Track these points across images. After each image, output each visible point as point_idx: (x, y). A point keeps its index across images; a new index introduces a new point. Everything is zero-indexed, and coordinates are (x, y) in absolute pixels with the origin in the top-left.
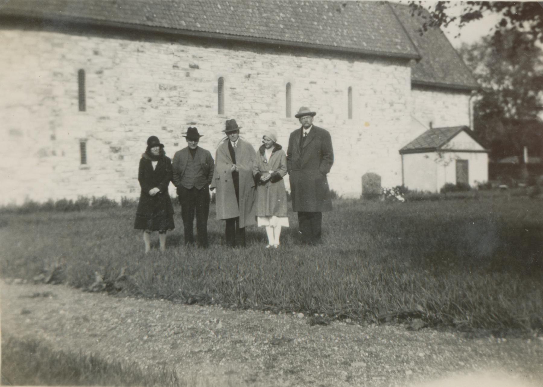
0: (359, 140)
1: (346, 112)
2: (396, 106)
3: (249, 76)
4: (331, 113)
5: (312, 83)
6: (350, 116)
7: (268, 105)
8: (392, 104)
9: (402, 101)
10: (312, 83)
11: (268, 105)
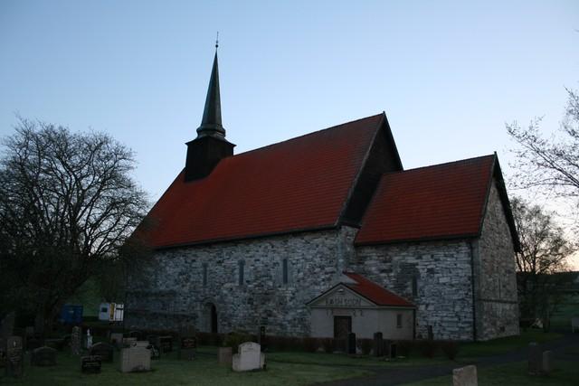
1: (281, 276)
3: (219, 262)
5: (256, 260)
6: (285, 280)
8: (322, 268)
10: (256, 260)
11: (229, 278)
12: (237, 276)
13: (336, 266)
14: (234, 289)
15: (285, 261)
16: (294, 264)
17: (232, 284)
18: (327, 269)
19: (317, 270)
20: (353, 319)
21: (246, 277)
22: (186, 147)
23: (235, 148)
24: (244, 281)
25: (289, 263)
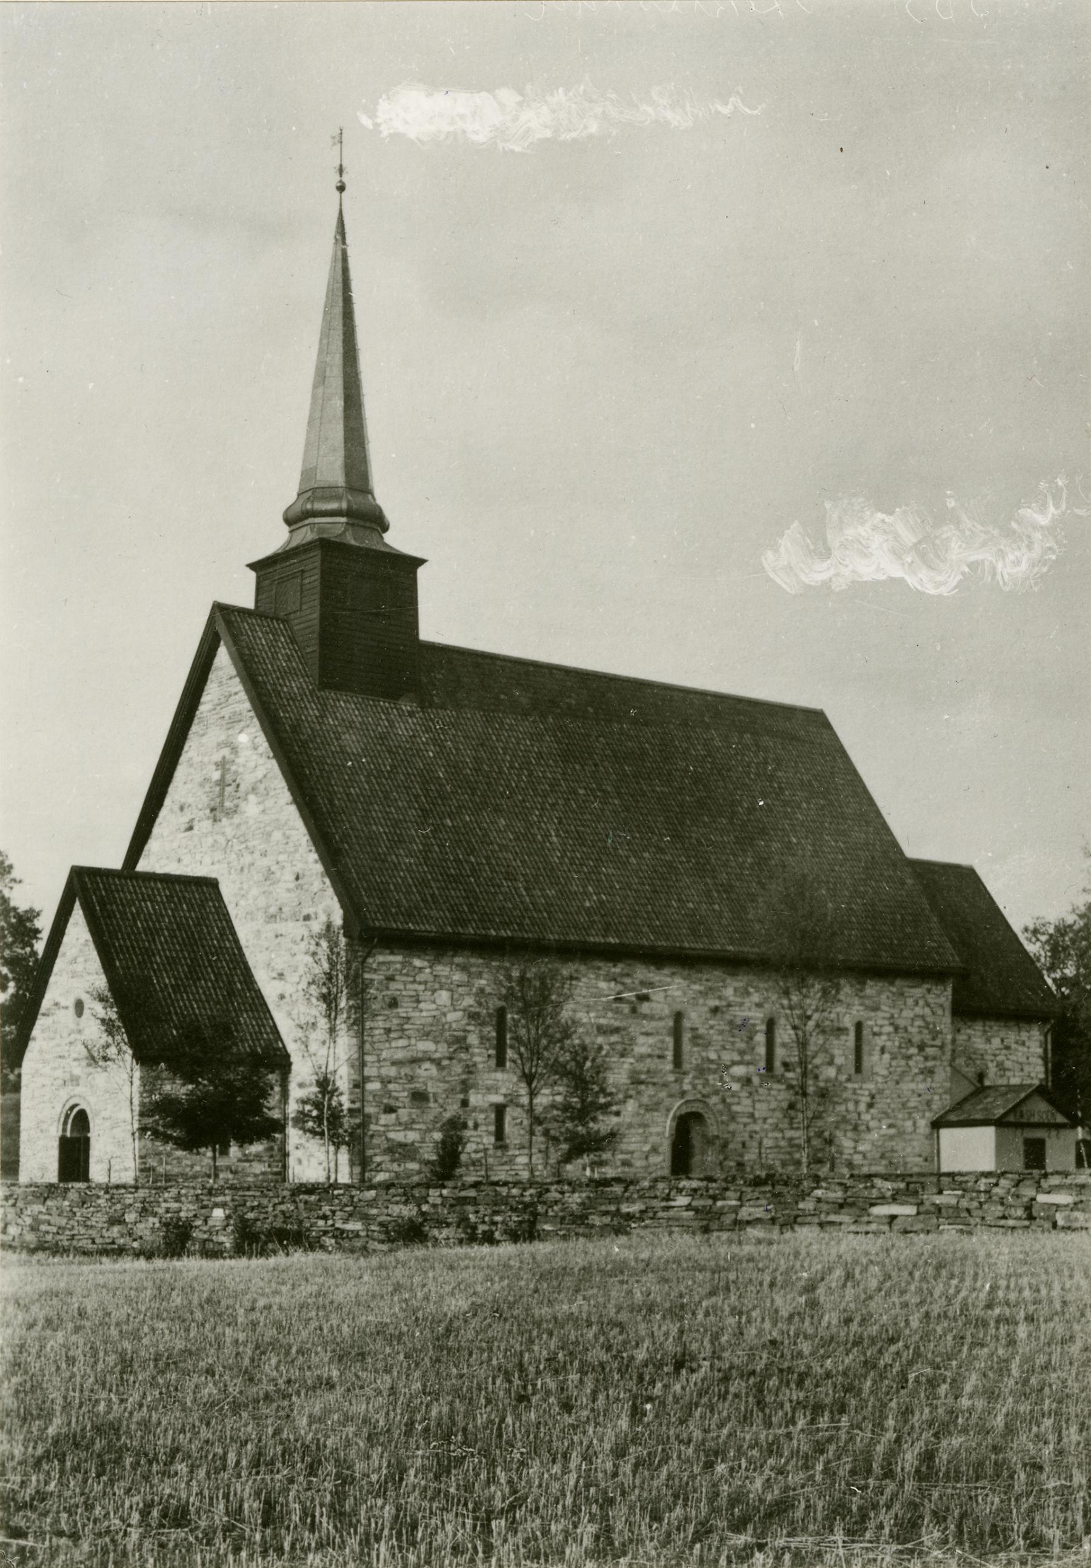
0: (870, 1106)
2: (930, 1051)
3: (715, 1010)
4: (831, 1063)
6: (858, 1069)
7: (742, 1053)
8: (921, 1047)
9: (938, 1042)
12: (762, 1050)
13: (942, 1047)
14: (756, 1080)
15: (859, 1026)
16: (875, 1034)
17: (752, 1069)
18: (930, 1051)
19: (913, 1051)
20: (1048, 1143)
21: (780, 1053)
22: (252, 575)
23: (421, 572)
24: (777, 1064)
25: (866, 1032)
